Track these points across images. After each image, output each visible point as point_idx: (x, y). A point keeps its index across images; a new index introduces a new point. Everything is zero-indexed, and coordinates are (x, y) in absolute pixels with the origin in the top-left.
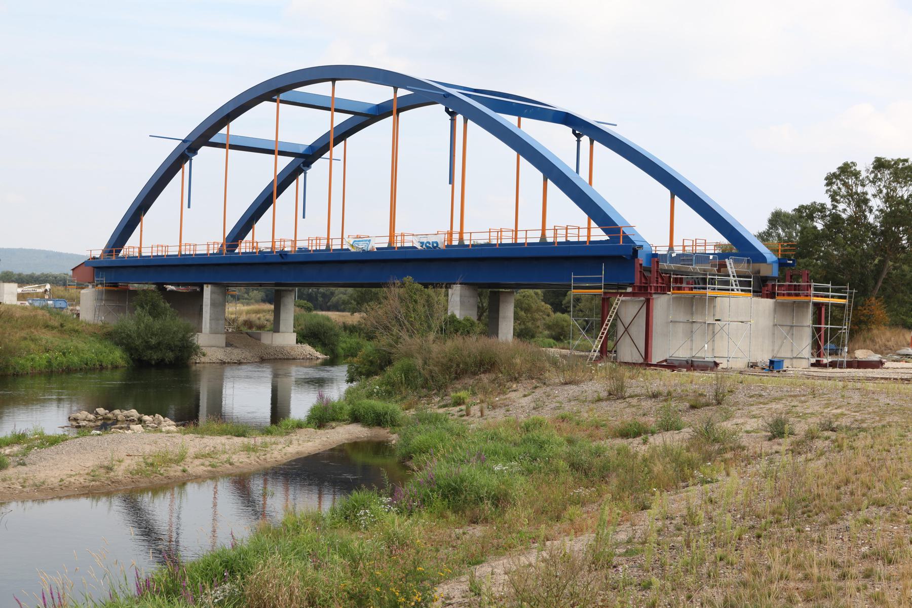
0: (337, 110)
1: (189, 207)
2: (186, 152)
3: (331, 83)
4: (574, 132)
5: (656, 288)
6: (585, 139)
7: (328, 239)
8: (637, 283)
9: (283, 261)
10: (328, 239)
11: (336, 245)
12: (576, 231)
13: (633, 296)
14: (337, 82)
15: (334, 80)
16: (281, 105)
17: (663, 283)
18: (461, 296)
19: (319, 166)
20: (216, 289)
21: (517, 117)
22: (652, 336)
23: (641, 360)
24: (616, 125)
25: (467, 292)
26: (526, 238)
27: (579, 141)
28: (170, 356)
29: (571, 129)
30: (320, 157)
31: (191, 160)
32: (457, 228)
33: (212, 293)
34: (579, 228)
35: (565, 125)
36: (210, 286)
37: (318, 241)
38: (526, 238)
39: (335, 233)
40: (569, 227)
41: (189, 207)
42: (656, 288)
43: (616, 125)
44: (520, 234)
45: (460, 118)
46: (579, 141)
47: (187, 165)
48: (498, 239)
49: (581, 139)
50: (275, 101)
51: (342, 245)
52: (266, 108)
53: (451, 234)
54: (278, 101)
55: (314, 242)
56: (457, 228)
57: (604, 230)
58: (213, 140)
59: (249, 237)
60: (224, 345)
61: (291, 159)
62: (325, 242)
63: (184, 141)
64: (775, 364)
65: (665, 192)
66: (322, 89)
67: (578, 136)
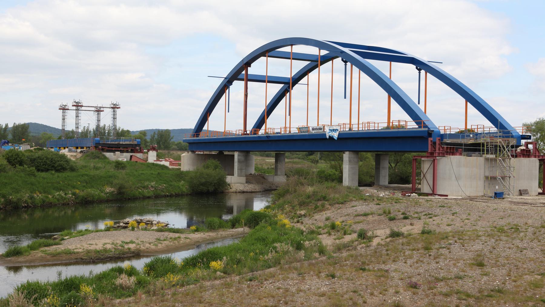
0: (293, 59)
1: (228, 112)
2: (227, 84)
3: (290, 47)
4: (417, 68)
5: (439, 153)
6: (423, 72)
7: (350, 124)
8: (429, 151)
9: (268, 139)
10: (350, 124)
11: (355, 128)
12: (373, 125)
13: (427, 158)
14: (293, 46)
15: (292, 45)
16: (268, 58)
17: (443, 151)
18: (349, 158)
19: (297, 90)
20: (241, 154)
21: (389, 62)
22: (436, 179)
23: (431, 192)
24: (442, 63)
25: (353, 155)
26: (378, 127)
27: (420, 73)
28: (211, 189)
29: (415, 67)
30: (297, 83)
31: (229, 87)
32: (288, 125)
33: (238, 156)
34: (375, 123)
35: (412, 64)
36: (237, 152)
37: (344, 126)
38: (378, 127)
39: (354, 121)
40: (394, 121)
41: (228, 112)
42: (439, 153)
43: (442, 63)
44: (361, 126)
45: (349, 64)
46: (420, 73)
47: (227, 91)
48: (369, 126)
49: (421, 71)
50: (265, 56)
51: (358, 128)
52: (263, 59)
53: (285, 128)
54: (267, 56)
55: (366, 125)
56: (288, 125)
57: (416, 123)
58: (239, 77)
59: (263, 127)
60: (245, 182)
61: (282, 85)
62: (349, 126)
63: (226, 78)
64: (497, 194)
65: (463, 100)
66: (287, 49)
67: (419, 70)
